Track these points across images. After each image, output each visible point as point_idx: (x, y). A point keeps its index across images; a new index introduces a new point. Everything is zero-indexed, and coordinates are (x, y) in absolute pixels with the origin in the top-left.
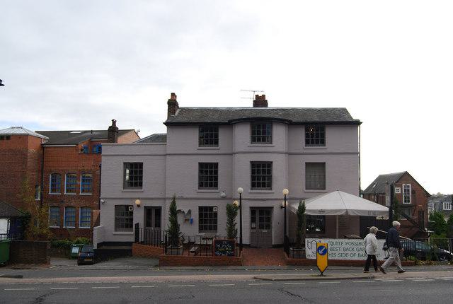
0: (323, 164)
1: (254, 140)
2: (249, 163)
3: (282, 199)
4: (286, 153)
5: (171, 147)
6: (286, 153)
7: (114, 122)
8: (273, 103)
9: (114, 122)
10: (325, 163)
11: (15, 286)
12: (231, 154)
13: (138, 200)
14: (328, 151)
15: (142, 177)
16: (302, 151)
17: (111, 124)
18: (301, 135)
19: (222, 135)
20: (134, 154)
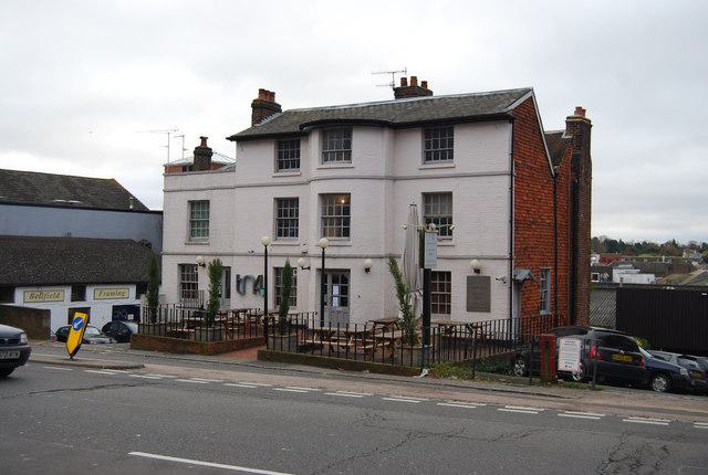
0: (448, 195)
1: (428, 157)
2: (420, 195)
3: (329, 257)
4: (387, 178)
5: (240, 177)
6: (387, 178)
7: (204, 140)
8: (287, 102)
9: (204, 140)
10: (297, 199)
11: (262, 393)
12: (395, 179)
13: (200, 254)
14: (457, 171)
15: (349, 218)
16: (415, 173)
17: (198, 143)
18: (414, 145)
19: (189, 157)
20: (200, 187)
